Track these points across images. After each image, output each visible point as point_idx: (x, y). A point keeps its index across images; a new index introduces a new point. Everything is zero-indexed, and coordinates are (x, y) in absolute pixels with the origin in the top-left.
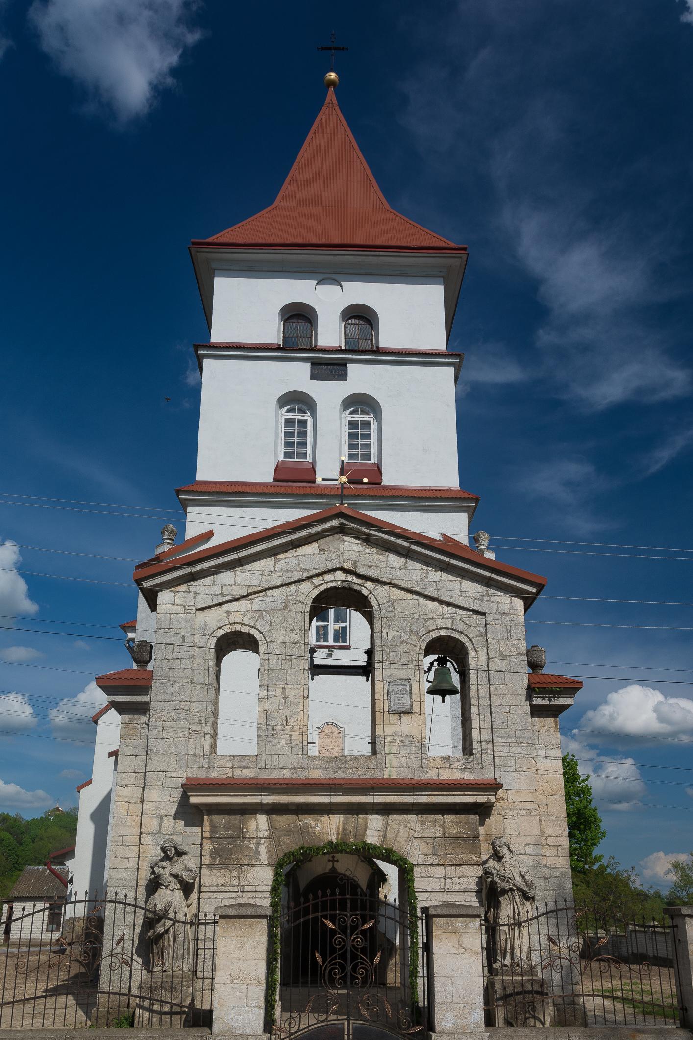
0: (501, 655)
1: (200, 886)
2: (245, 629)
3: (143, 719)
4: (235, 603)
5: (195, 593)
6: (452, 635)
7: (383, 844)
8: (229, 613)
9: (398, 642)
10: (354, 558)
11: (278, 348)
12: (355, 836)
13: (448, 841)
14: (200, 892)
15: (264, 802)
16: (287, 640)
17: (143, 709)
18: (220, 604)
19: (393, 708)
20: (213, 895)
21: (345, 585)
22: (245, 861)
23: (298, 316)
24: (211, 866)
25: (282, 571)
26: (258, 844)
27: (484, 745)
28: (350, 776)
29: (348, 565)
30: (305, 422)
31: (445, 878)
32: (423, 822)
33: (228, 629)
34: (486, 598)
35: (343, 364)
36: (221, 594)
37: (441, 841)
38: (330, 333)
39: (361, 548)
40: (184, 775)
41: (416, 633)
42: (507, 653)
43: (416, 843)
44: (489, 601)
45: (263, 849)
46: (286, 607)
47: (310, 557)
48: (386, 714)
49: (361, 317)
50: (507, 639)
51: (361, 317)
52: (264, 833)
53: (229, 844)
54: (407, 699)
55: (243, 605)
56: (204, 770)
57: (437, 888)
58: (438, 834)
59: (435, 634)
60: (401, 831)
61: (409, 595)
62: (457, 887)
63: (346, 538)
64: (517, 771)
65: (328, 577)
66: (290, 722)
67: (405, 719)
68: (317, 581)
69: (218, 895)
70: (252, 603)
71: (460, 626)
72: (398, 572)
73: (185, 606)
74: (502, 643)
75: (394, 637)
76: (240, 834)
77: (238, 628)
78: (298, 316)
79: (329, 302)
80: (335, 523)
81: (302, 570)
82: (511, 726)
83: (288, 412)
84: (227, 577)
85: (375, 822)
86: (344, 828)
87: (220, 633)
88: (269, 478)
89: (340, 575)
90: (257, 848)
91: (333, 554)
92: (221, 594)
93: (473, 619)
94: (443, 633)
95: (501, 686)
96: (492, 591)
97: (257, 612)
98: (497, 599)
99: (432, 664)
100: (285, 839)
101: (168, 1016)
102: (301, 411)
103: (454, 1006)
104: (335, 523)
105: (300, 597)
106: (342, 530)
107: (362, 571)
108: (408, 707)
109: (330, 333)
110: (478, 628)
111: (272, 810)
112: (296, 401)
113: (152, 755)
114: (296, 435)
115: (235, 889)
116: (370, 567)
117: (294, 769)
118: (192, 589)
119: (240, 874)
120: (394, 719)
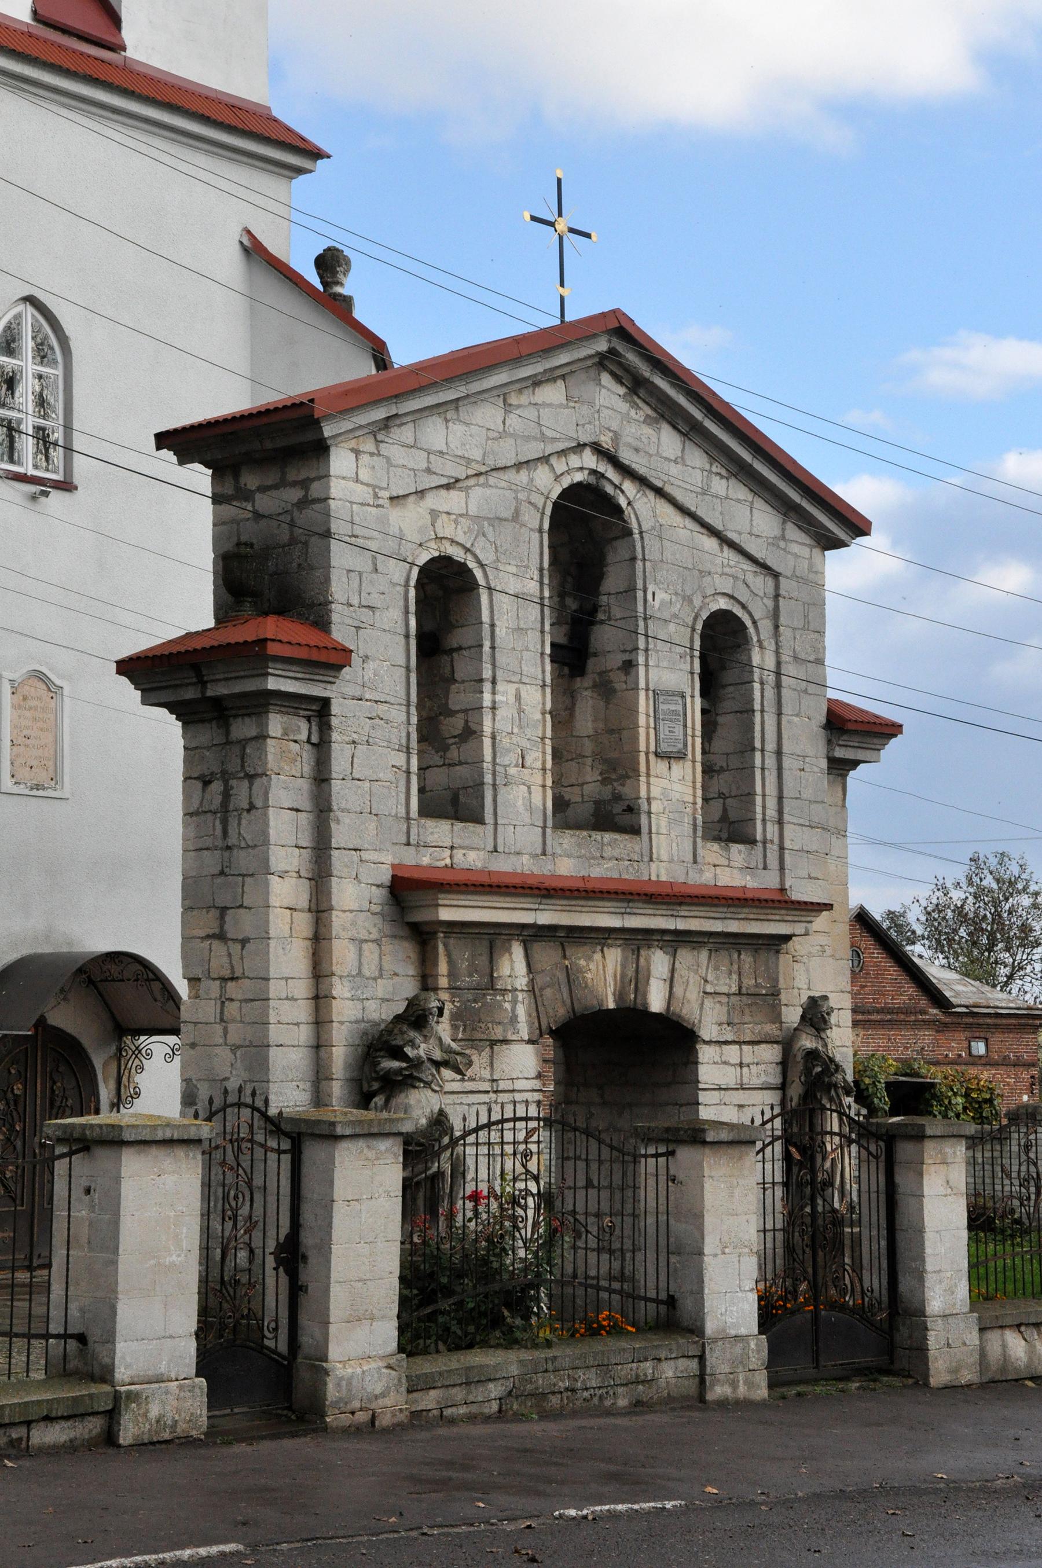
4: (443, 492)
5: (388, 459)
6: (734, 611)
8: (434, 514)
9: (666, 615)
13: (744, 998)
15: (540, 922)
17: (320, 711)
19: (664, 747)
21: (592, 480)
22: (498, 1033)
26: (515, 1002)
28: (609, 874)
29: (606, 441)
34: (782, 544)
36: (428, 471)
37: (734, 999)
39: (623, 406)
40: (388, 859)
42: (803, 656)
43: (708, 1002)
44: (784, 550)
45: (521, 1011)
46: (516, 516)
48: (652, 757)
50: (803, 629)
52: (522, 982)
53: (475, 1001)
54: (679, 731)
55: (453, 501)
56: (412, 850)
60: (691, 981)
64: (810, 878)
66: (528, 763)
67: (677, 768)
68: (560, 466)
70: (467, 496)
71: (743, 595)
73: (374, 487)
81: (543, 438)
82: (804, 796)
85: (659, 962)
89: (589, 460)
90: (514, 1010)
91: (585, 410)
93: (761, 584)
95: (796, 719)
96: (793, 532)
97: (477, 519)
98: (795, 548)
101: (15, 1330)
103: (942, 1275)
107: (626, 456)
110: (765, 600)
111: (533, 935)
113: (339, 814)
115: (486, 1086)
116: (637, 450)
117: (534, 856)
119: (492, 1057)
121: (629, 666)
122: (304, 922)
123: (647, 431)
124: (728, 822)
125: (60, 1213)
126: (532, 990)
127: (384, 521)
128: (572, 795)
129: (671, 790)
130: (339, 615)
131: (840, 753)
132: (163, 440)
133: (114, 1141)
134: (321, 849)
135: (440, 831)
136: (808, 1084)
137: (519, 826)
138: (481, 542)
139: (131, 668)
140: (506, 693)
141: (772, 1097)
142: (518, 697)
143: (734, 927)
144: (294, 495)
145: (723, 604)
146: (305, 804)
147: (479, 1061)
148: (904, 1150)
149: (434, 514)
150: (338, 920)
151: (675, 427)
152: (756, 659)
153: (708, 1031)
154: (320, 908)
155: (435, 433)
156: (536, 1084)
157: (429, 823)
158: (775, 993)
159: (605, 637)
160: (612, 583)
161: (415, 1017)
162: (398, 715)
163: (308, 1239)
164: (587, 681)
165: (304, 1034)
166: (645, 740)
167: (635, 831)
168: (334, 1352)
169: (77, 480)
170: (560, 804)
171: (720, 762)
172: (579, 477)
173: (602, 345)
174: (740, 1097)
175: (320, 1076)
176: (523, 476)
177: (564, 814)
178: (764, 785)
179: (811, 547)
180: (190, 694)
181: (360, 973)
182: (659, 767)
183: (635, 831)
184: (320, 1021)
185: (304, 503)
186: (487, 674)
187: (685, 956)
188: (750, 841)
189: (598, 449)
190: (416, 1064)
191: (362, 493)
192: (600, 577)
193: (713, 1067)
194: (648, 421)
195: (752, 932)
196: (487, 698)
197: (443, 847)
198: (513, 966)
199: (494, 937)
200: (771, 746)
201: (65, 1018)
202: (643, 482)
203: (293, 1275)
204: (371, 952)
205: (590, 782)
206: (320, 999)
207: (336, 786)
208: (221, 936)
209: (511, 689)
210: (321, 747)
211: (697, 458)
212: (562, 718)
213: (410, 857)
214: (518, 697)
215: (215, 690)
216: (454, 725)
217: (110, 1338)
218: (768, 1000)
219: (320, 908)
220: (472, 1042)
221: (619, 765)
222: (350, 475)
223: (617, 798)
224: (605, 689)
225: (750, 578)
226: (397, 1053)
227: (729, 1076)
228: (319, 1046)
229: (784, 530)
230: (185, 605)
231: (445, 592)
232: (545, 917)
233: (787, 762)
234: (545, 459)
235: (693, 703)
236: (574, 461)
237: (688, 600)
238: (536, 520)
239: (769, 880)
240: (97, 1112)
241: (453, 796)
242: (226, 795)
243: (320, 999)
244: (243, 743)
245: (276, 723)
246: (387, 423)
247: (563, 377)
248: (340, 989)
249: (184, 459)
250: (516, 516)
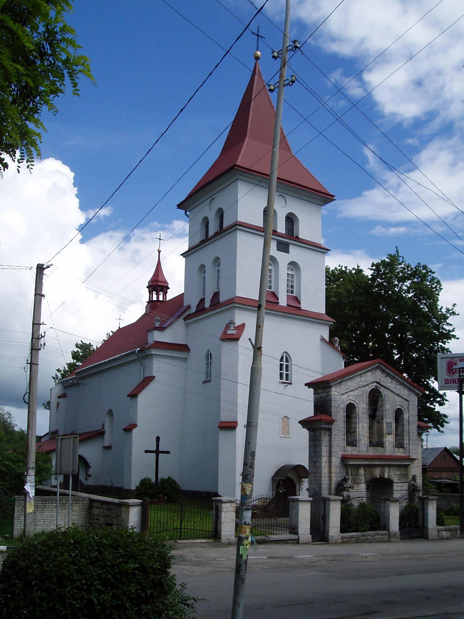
8: (349, 395)
17: (330, 430)
29: (378, 381)
39: (381, 374)
45: (363, 478)
46: (363, 394)
55: (352, 393)
61: (391, 393)
67: (391, 436)
68: (370, 386)
71: (402, 405)
76: (358, 474)
81: (367, 381)
85: (387, 470)
89: (375, 384)
93: (406, 403)
96: (411, 393)
97: (356, 396)
107: (381, 383)
111: (365, 466)
121: (382, 419)
122: (327, 464)
123: (385, 378)
124: (399, 444)
125: (291, 510)
126: (365, 475)
127: (340, 398)
128: (373, 440)
129: (389, 439)
130: (333, 414)
131: (420, 432)
132: (306, 385)
133: (298, 500)
134: (330, 452)
135: (350, 449)
136: (412, 489)
137: (363, 447)
140: (361, 424)
141: (407, 492)
143: (400, 463)
144: (326, 394)
145: (399, 407)
146: (328, 445)
147: (356, 487)
148: (426, 501)
149: (349, 395)
150: (333, 464)
152: (405, 416)
153: (395, 481)
154: (330, 462)
155: (349, 383)
157: (347, 447)
158: (407, 474)
159: (378, 413)
160: (379, 404)
161: (345, 480)
162: (343, 429)
163: (326, 515)
164: (376, 421)
165: (327, 482)
166: (385, 431)
167: (383, 447)
168: (330, 532)
169: (292, 382)
170: (370, 442)
171: (399, 434)
172: (373, 387)
173: (377, 365)
174: (401, 492)
175: (330, 489)
176: (364, 388)
177: (371, 444)
178: (406, 438)
180: (310, 427)
182: (388, 436)
183: (383, 447)
184: (330, 480)
185: (328, 395)
186: (358, 422)
187: (391, 468)
188: (403, 448)
189: (376, 382)
190: (345, 487)
191: (337, 393)
192: (378, 403)
193: (396, 487)
194: (385, 376)
195: (403, 464)
196: (358, 426)
197: (351, 451)
198: (362, 471)
199: (358, 467)
200: (407, 431)
201: (290, 475)
202: (384, 387)
203: (324, 521)
204: (338, 469)
205: (376, 439)
206: (330, 477)
207: (332, 442)
208: (314, 466)
210: (330, 436)
211: (394, 382)
212: (371, 428)
213: (344, 453)
215: (313, 427)
216: (353, 430)
217: (298, 528)
218: (406, 475)
219: (330, 462)
220: (354, 483)
221: (381, 436)
222: (335, 392)
223: (380, 441)
224: (378, 422)
226: (342, 486)
227: (399, 489)
228: (330, 484)
230: (309, 411)
231: (350, 408)
232: (367, 463)
233: (410, 434)
236: (373, 384)
237: (392, 407)
238: (366, 395)
239: (407, 454)
240: (266, 309)
241: (352, 442)
242: (315, 443)
243: (330, 477)
244: (318, 435)
245: (323, 432)
246: (341, 382)
248: (333, 475)
249: (309, 388)
250: (363, 394)
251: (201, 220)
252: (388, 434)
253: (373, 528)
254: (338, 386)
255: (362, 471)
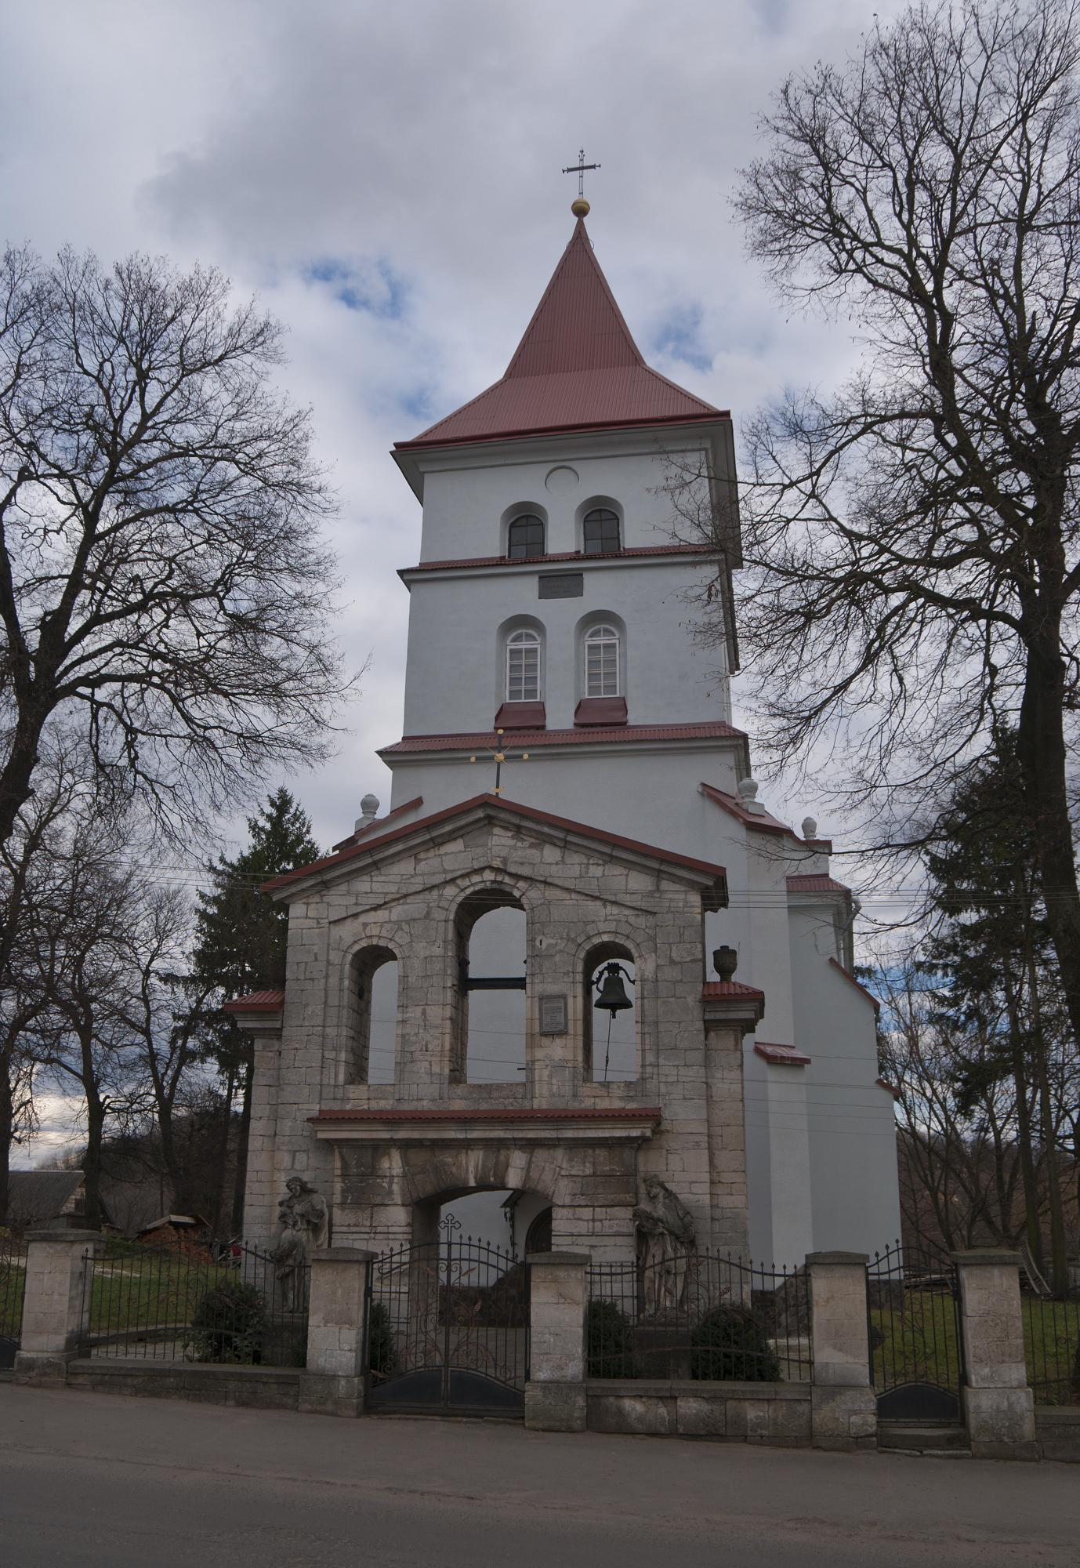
0: (672, 962)
1: (331, 1225)
2: (382, 943)
3: (276, 1045)
7: (525, 1183)
8: (365, 925)
10: (503, 854)
11: (500, 562)
12: (495, 1175)
14: (331, 1232)
16: (428, 953)
17: (277, 1034)
18: (355, 916)
19: (546, 1029)
20: (345, 1236)
21: (495, 886)
22: (378, 1200)
23: (525, 522)
24: (342, 1205)
25: (423, 875)
26: (391, 1183)
27: (649, 1069)
28: (495, 1107)
29: (497, 863)
30: (535, 650)
31: (593, 1220)
32: (571, 1160)
33: (364, 944)
35: (578, 575)
36: (356, 904)
38: (563, 536)
39: (512, 842)
41: (574, 940)
43: (563, 1183)
47: (455, 856)
49: (601, 516)
51: (601, 516)
54: (561, 1018)
55: (382, 915)
57: (584, 1232)
58: (588, 1172)
59: (596, 941)
61: (566, 896)
62: (607, 1230)
63: (497, 831)
65: (476, 879)
66: (430, 1047)
67: (558, 1042)
69: (350, 1236)
71: (625, 929)
72: (554, 868)
74: (674, 948)
75: (549, 945)
76: (373, 1172)
77: (375, 942)
78: (525, 522)
79: (562, 501)
80: (480, 814)
81: (445, 871)
83: (514, 640)
84: (363, 885)
85: (518, 1158)
86: (484, 1166)
87: (357, 948)
88: (489, 727)
89: (489, 876)
90: (390, 1187)
91: (479, 851)
92: (356, 904)
93: (642, 921)
94: (605, 938)
96: (665, 885)
99: (601, 973)
100: (419, 1177)
102: (530, 637)
104: (480, 814)
105: (444, 904)
106: (490, 821)
107: (512, 869)
108: (561, 1027)
109: (563, 536)
111: (406, 1145)
112: (521, 624)
114: (523, 669)
117: (433, 1100)
118: (325, 899)
120: (545, 1041)
138: (400, 933)
139: (380, 753)
142: (424, 1012)
151: (555, 845)
156: (408, 1229)
179: (686, 892)
181: (292, 1167)
187: (540, 1155)
194: (532, 846)
198: (393, 1164)
199: (379, 1148)
209: (419, 1010)
214: (424, 1012)
225: (632, 920)
229: (658, 886)
234: (453, 881)
235: (575, 1003)
247: (462, 836)
251: (505, 507)
252: (544, 1034)
253: (763, 1379)
254: (317, 899)
255: (393, 1164)
